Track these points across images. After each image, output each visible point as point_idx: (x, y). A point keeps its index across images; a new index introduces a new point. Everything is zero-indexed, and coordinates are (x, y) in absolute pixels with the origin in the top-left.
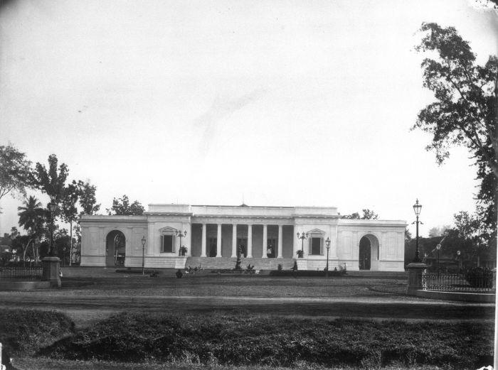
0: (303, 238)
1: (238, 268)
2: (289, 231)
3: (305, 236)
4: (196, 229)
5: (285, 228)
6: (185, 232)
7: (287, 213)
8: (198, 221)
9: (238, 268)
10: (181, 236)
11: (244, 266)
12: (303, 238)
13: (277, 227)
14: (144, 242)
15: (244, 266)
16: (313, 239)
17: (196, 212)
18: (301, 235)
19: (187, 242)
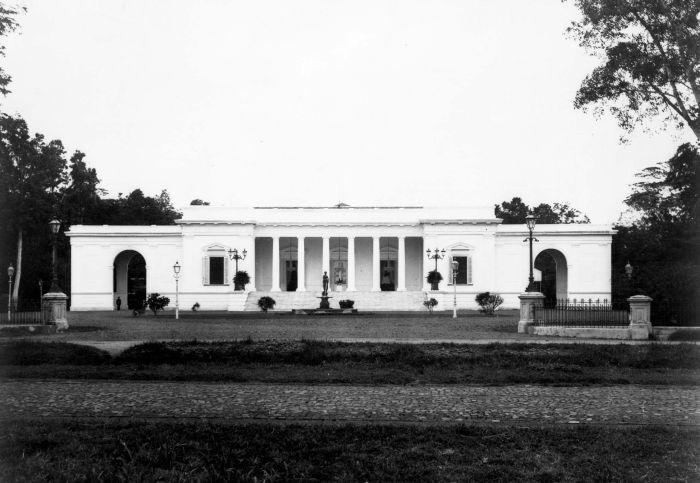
0: (436, 257)
2: (415, 245)
3: (440, 254)
4: (263, 246)
7: (415, 217)
8: (264, 233)
9: (325, 303)
10: (237, 258)
14: (177, 269)
17: (261, 217)
18: (433, 253)
19: (248, 265)
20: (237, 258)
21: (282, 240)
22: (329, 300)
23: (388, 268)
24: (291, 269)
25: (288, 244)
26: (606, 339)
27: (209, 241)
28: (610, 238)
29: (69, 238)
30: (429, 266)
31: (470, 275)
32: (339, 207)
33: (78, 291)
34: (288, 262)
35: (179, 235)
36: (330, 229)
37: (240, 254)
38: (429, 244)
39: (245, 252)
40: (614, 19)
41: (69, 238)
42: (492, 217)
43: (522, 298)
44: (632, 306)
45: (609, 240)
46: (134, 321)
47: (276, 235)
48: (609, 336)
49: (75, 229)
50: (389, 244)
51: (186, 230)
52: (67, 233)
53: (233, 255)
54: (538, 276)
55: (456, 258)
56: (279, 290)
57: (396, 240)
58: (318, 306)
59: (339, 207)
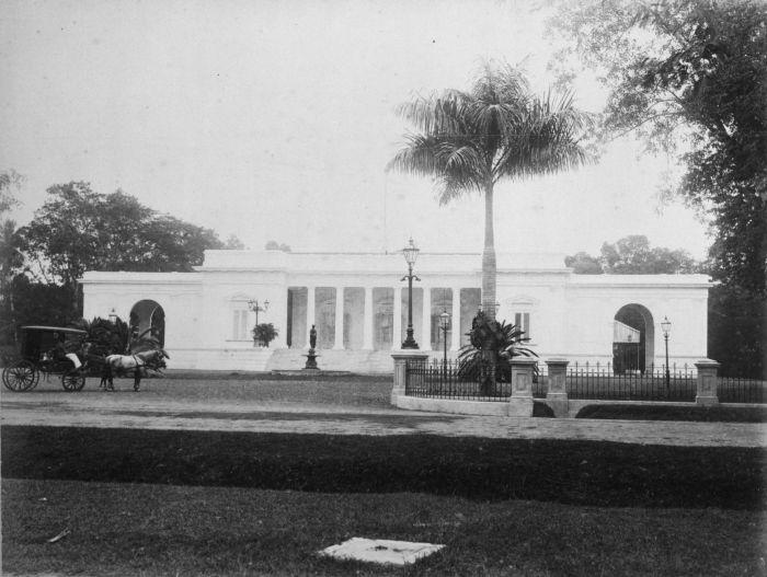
4: (295, 298)
5: (434, 291)
8: (297, 283)
10: (256, 309)
20: (256, 309)
22: (317, 359)
24: (385, 323)
25: (325, 296)
26: (407, 410)
28: (707, 292)
29: (81, 285)
33: (677, 354)
35: (200, 284)
37: (261, 305)
41: (81, 285)
42: (562, 265)
43: (700, 367)
44: (514, 372)
45: (705, 294)
47: (312, 285)
48: (424, 408)
49: (89, 276)
52: (79, 281)
57: (305, 290)
58: (304, 366)
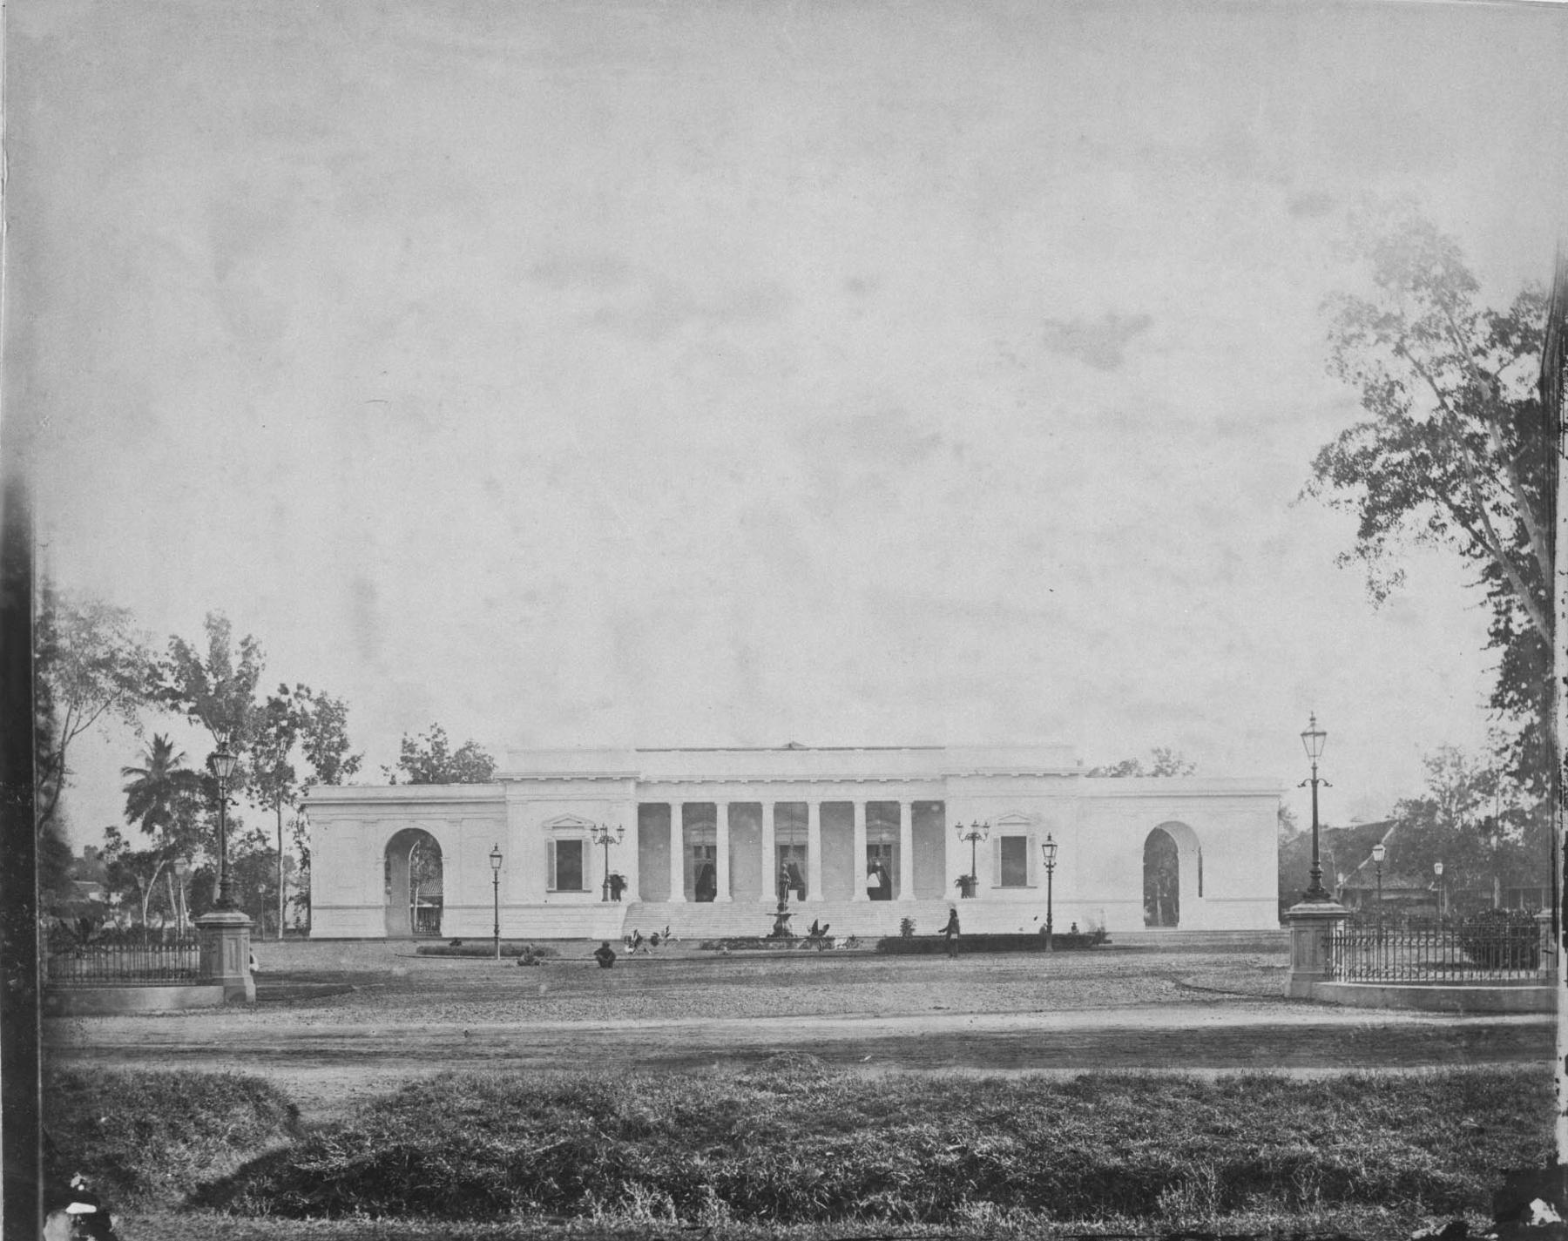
0: (974, 837)
1: (780, 933)
2: (928, 814)
3: (981, 832)
4: (652, 816)
5: (687, 808)
6: (621, 830)
8: (654, 796)
9: (780, 933)
10: (606, 840)
11: (799, 927)
12: (974, 837)
13: (665, 808)
15: (799, 927)
16: (1003, 838)
17: (651, 768)
18: (968, 830)
19: (625, 859)
21: (687, 808)
23: (792, 858)
25: (698, 815)
27: (557, 811)
30: (957, 864)
31: (550, 866)
32: (790, 747)
34: (698, 849)
35: (502, 802)
36: (729, 788)
37: (612, 833)
38: (952, 816)
39: (621, 830)
40: (1420, 821)
46: (458, 935)
50: (883, 813)
51: (513, 792)
53: (599, 835)
54: (1519, 378)
55: (1006, 840)
56: (684, 900)
59: (790, 747)
